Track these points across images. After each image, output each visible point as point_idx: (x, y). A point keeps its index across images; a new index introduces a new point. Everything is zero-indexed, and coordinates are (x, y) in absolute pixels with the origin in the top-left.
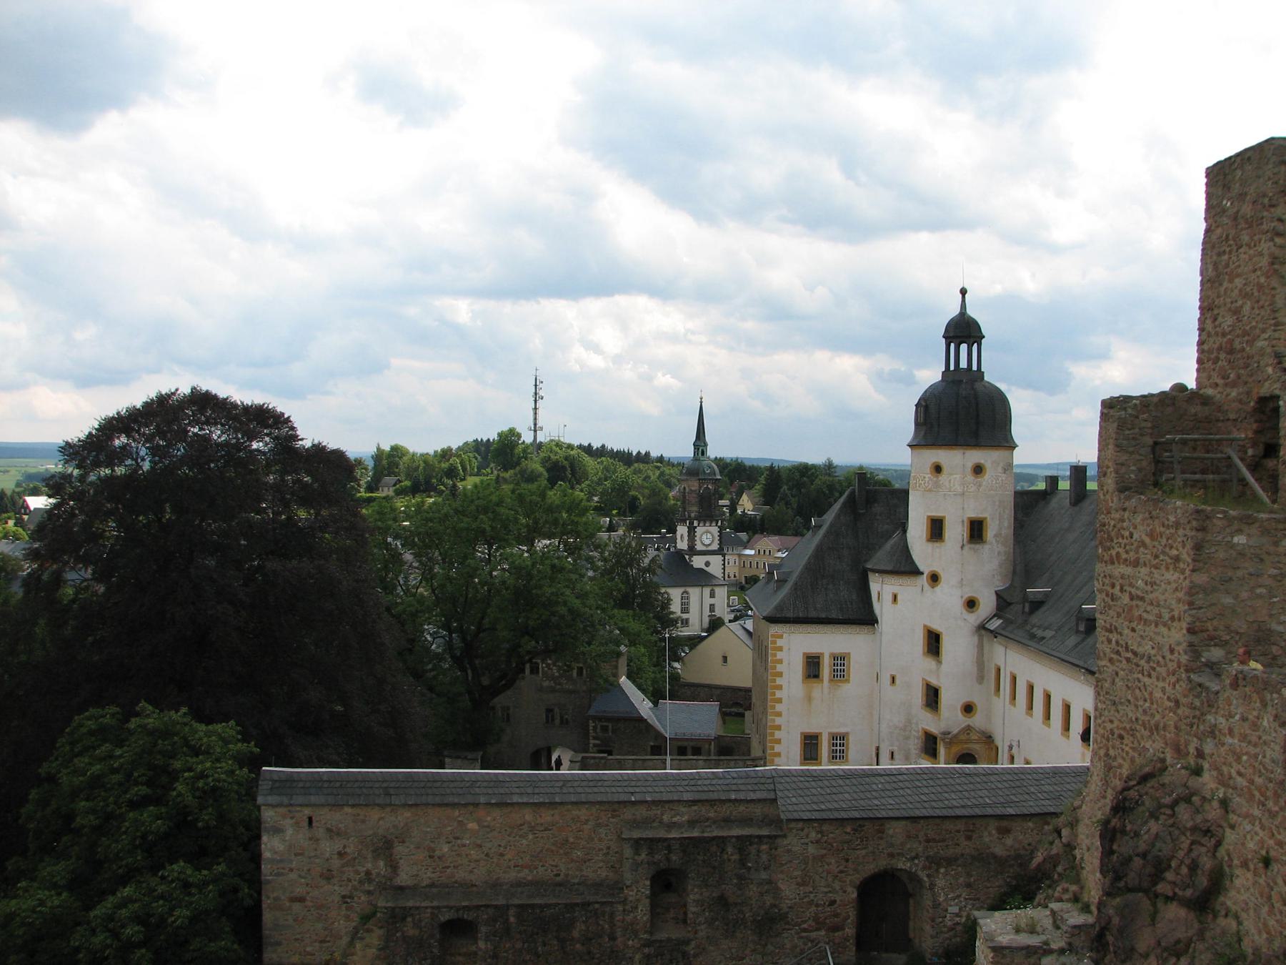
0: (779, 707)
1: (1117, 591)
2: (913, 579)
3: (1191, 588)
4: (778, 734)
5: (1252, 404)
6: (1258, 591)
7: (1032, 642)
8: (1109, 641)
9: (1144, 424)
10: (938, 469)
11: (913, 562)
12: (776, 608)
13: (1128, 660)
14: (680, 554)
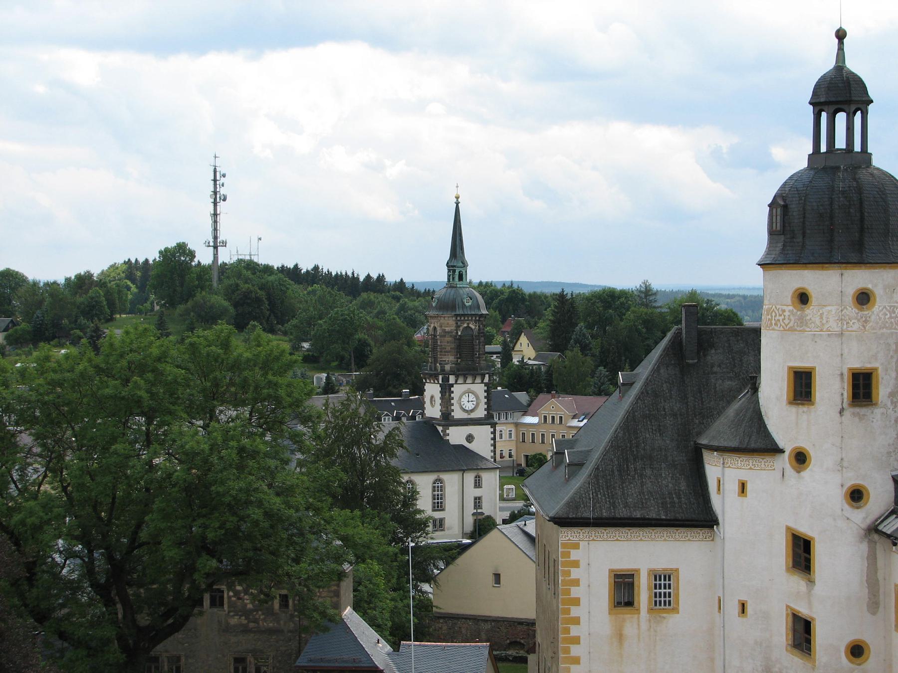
10: (803, 298)
12: (568, 504)
14: (430, 424)
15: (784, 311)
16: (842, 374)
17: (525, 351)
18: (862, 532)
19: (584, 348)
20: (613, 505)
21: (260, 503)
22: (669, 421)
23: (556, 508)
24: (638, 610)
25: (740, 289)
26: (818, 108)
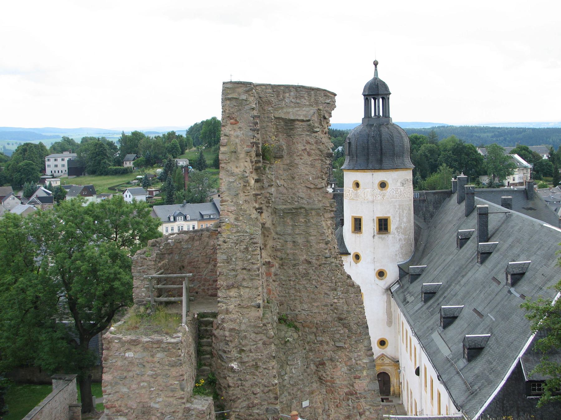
6: (142, 384)
9: (150, 263)
10: (357, 185)
18: (384, 290)
21: (119, 280)
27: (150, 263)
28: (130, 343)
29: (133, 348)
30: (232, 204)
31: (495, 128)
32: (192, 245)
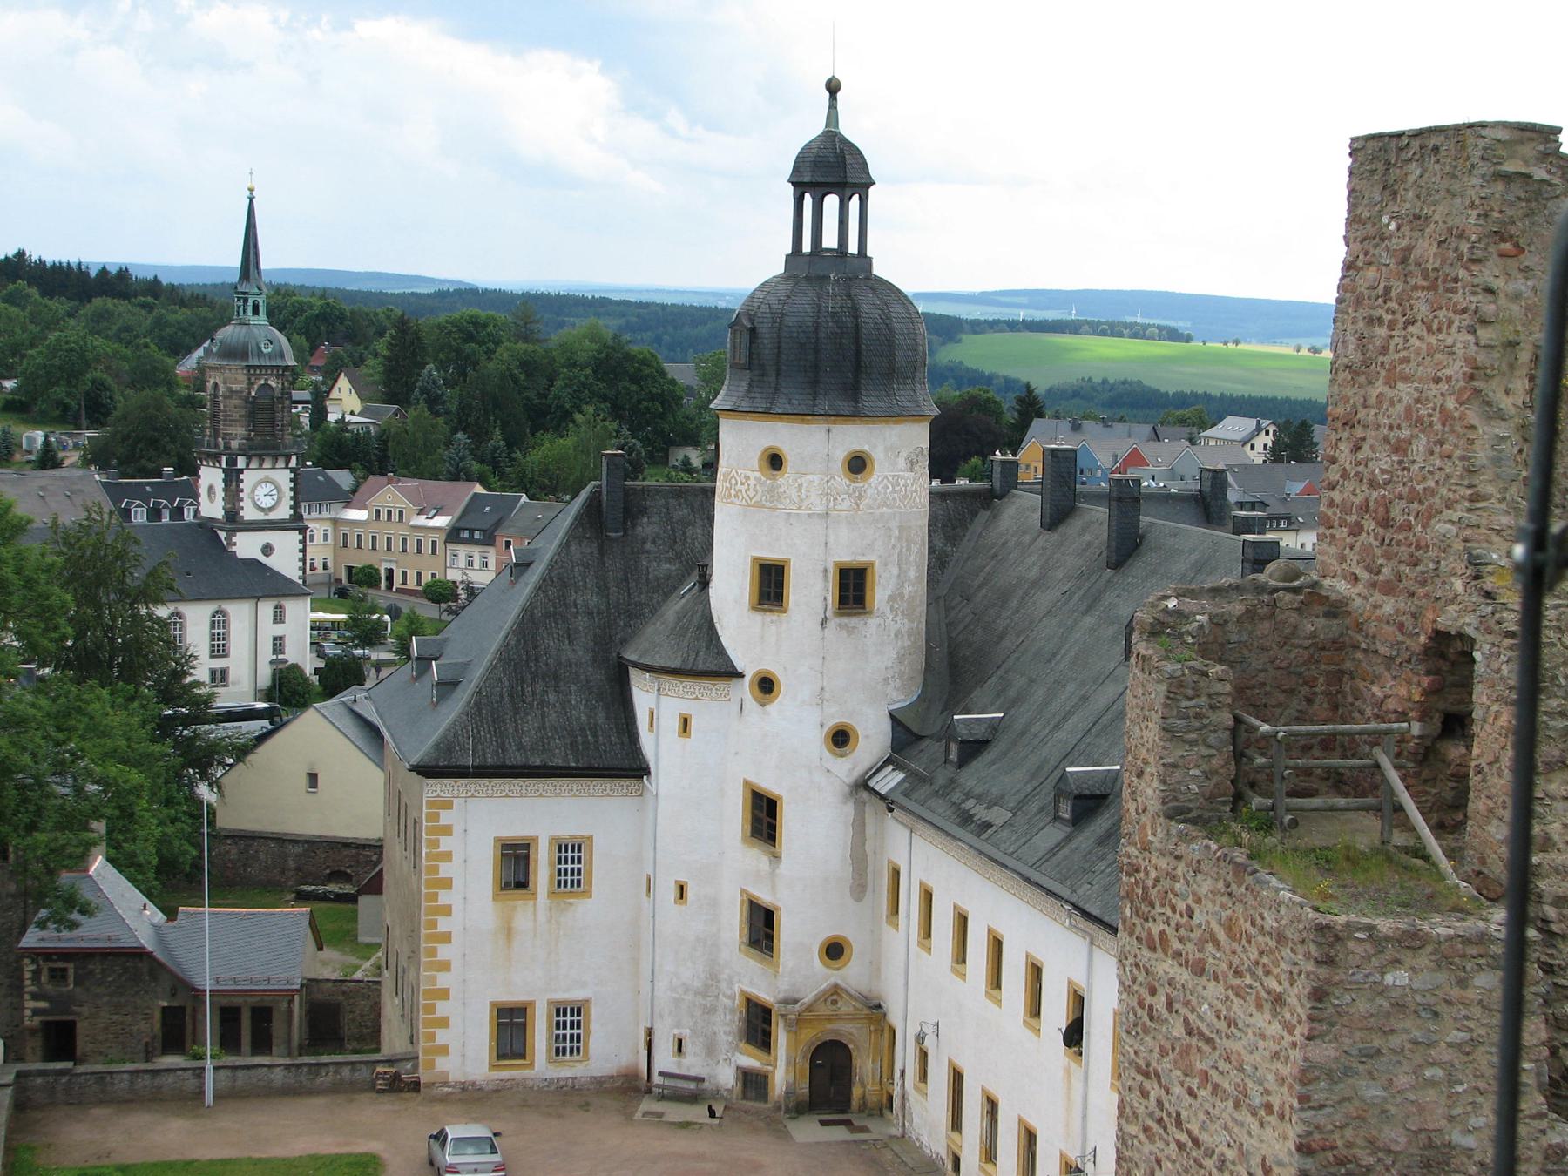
0: (444, 952)
1: (1159, 1002)
2: (721, 684)
3: (1304, 1071)
4: (442, 1009)
5: (1422, 639)
6: (1428, 1073)
7: (968, 827)
8: (1145, 1094)
9: (1219, 687)
10: (775, 461)
11: (721, 652)
12: (437, 745)
13: (1181, 1146)
14: (206, 527)
15: (747, 478)
16: (826, 571)
17: (346, 403)
19: (433, 401)
20: (502, 746)
22: (582, 623)
23: (420, 752)
24: (535, 894)
25: (658, 291)
26: (800, 191)
27: (1219, 687)
28: (1399, 941)
29: (1407, 957)
30: (1503, 506)
31: (627, 303)
32: (1251, 633)
